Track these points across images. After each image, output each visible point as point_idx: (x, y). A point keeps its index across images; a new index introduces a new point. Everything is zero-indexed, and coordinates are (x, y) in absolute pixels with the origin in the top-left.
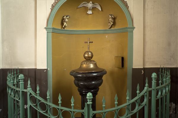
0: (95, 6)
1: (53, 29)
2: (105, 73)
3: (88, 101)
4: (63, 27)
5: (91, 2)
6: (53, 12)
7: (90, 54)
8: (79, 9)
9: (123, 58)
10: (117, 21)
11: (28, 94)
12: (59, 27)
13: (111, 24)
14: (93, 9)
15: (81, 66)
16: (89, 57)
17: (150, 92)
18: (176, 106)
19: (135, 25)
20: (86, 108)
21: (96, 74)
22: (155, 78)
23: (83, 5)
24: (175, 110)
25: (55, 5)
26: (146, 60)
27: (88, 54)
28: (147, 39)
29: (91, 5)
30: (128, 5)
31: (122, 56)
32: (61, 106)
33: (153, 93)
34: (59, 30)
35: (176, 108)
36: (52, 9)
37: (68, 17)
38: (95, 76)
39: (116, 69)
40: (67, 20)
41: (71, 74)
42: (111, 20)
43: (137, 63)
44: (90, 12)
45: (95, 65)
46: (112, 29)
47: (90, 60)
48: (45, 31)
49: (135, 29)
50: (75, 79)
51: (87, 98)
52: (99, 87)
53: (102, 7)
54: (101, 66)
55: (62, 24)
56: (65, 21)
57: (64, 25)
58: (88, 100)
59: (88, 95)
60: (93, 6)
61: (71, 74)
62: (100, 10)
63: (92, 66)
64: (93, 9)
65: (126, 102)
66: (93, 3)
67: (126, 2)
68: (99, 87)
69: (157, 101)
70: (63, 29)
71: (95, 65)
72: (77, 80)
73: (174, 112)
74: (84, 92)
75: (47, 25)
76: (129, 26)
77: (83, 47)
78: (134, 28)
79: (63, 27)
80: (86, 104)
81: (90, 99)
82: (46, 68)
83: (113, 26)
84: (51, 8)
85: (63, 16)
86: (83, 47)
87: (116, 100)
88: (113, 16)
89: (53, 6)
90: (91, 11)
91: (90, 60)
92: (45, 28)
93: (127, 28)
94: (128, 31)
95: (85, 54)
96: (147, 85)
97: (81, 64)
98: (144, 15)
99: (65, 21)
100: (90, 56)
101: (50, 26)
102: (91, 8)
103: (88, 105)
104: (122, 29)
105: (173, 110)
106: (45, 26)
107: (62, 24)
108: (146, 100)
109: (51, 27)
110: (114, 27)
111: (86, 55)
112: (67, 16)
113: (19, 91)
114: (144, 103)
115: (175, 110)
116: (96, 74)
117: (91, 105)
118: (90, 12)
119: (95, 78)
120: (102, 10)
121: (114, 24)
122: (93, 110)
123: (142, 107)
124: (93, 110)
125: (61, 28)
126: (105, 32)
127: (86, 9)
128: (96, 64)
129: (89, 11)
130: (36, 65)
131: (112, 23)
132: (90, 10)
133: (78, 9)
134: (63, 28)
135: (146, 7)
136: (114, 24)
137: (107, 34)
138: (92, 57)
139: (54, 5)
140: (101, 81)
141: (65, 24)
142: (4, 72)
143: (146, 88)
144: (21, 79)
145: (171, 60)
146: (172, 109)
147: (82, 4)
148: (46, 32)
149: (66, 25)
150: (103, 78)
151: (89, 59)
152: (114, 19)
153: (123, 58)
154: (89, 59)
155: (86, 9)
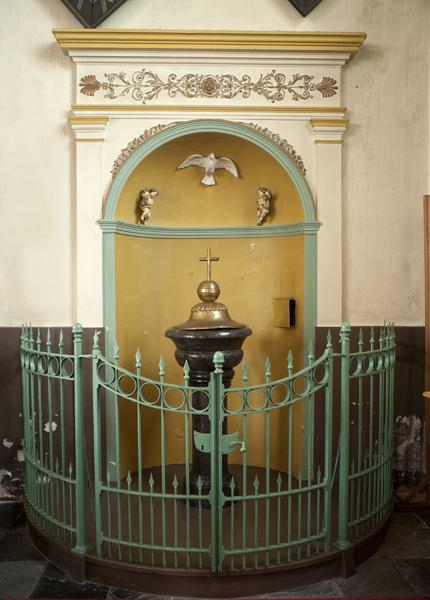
0: (222, 165)
1: (119, 224)
2: (250, 333)
3: (215, 369)
4: (142, 218)
5: (212, 156)
6: (117, 179)
7: (212, 286)
8: (181, 171)
9: (293, 303)
10: (278, 204)
11: (95, 362)
12: (131, 219)
13: (263, 214)
14: (219, 172)
15: (191, 316)
16: (210, 295)
17: (337, 362)
18: (422, 422)
19: (321, 219)
20: (212, 383)
21: (227, 334)
22: (347, 332)
23: (190, 163)
24: (421, 434)
25: (124, 162)
26: (351, 306)
27: (209, 288)
28: (353, 254)
29: (211, 162)
30: (306, 166)
31: (290, 297)
32: (102, 491)
33: (345, 364)
34: (132, 226)
35: (421, 429)
36: (115, 175)
37: (153, 193)
38: (224, 338)
39: (278, 332)
40: (150, 201)
41: (170, 334)
42: (262, 201)
43: (326, 312)
44: (209, 181)
45: (225, 313)
46: (266, 225)
47: (212, 301)
48: (98, 231)
49: (321, 228)
50: (178, 347)
51: (214, 361)
52: (234, 368)
53: (241, 168)
54: (238, 318)
55: (139, 211)
56: (146, 204)
57: (145, 213)
58: (216, 366)
59: (215, 356)
60: (217, 163)
61: (170, 334)
62: (236, 175)
63: (217, 315)
64: (219, 172)
65: (287, 376)
66: (216, 157)
67: (299, 158)
68: (234, 368)
69: (353, 382)
70: (139, 223)
71: (225, 313)
72: (181, 349)
73: (418, 439)
74: (199, 379)
75: (103, 217)
76: (306, 221)
77: (192, 274)
78: (319, 225)
79: (142, 218)
80: (212, 374)
81: (219, 364)
82: (101, 326)
83: (269, 218)
84: (111, 169)
85: (140, 190)
86: (192, 274)
87: (268, 370)
88: (267, 193)
89: (118, 166)
90: (212, 178)
91: (212, 301)
92: (100, 223)
93: (301, 225)
94: (300, 236)
95: (200, 287)
96: (329, 345)
97: (192, 312)
98: (342, 191)
99: (146, 204)
100: (213, 292)
101: (111, 217)
102: (213, 171)
103: (216, 375)
104: (292, 226)
105: (414, 435)
106: (98, 217)
107: (139, 211)
108: (328, 376)
109: (113, 219)
110: (271, 221)
111: (203, 291)
112: (150, 191)
113: (73, 359)
114: (324, 381)
115: (421, 434)
116: (227, 334)
117: (221, 376)
118: (209, 181)
119: (221, 344)
120: (240, 176)
121: (272, 212)
122: (226, 388)
123: (319, 387)
124: (226, 388)
125: (137, 222)
126: (245, 234)
127: (200, 172)
128: (226, 311)
129: (207, 177)
130: (74, 316)
131: (265, 211)
132: (209, 174)
133: (179, 173)
134: (139, 223)
135: (349, 171)
136: (272, 212)
137: (252, 240)
138: (216, 297)
139: (120, 162)
140: (237, 353)
141: (146, 211)
142: (10, 335)
143: (327, 351)
144: (78, 333)
145: (410, 307)
146: (413, 431)
147: (190, 160)
148: (101, 231)
149: (149, 214)
150: (243, 348)
151: (210, 300)
152: (271, 199)
153: (293, 303)
154: (210, 300)
155: (200, 172)
